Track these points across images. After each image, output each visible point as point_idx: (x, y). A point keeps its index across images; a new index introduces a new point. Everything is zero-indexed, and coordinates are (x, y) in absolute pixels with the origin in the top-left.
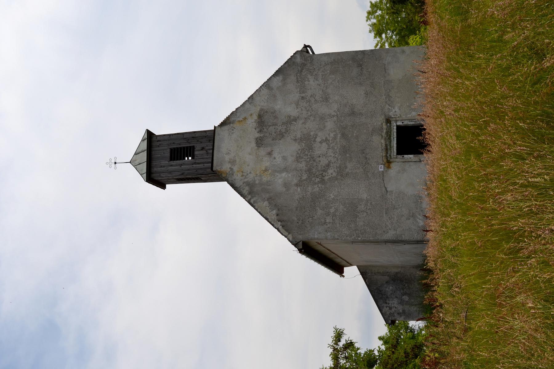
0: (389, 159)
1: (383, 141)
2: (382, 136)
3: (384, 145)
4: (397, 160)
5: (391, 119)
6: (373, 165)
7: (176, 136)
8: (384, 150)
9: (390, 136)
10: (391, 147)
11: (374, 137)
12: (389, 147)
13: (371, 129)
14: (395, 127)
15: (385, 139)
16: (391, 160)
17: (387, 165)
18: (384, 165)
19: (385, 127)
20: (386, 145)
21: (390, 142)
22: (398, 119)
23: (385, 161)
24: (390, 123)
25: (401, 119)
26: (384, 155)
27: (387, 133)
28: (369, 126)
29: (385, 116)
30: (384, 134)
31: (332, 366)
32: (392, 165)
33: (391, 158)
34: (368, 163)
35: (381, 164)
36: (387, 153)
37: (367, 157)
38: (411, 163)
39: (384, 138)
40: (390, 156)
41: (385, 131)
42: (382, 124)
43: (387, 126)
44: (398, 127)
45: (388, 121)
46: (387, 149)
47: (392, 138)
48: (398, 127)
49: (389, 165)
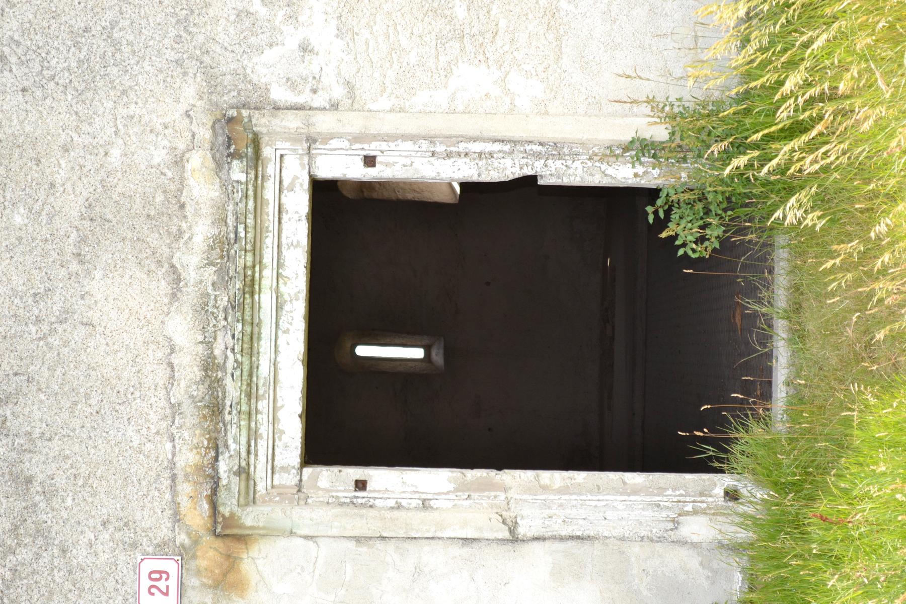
0: (228, 505)
1: (182, 329)
2: (176, 277)
3: (189, 369)
4: (304, 518)
5: (261, 122)
6: (80, 555)
7: (417, 363)
8: (190, 416)
9: (251, 287)
10: (251, 393)
11: (97, 285)
12: (233, 390)
13: (72, 206)
14: (299, 203)
15: (203, 308)
16: (249, 518)
17: (210, 554)
18: (185, 554)
19: (202, 187)
20: (210, 367)
21: (249, 343)
22: (324, 123)
23: (197, 516)
24: (256, 160)
25: (354, 123)
26: (188, 458)
27: (223, 248)
28: (61, 170)
29: (212, 83)
30: (192, 261)
31: (541, 182)
32: (260, 562)
33: (249, 497)
34: (41, 532)
35: (162, 549)
36: (216, 447)
37: (34, 466)
38: (434, 557)
39: (190, 295)
40: (244, 472)
41: (202, 231)
42: (179, 162)
43: (227, 187)
44: (324, 192)
45: (238, 140)
46: (215, 409)
47: (266, 300)
48: (324, 192)
49: (231, 563)
